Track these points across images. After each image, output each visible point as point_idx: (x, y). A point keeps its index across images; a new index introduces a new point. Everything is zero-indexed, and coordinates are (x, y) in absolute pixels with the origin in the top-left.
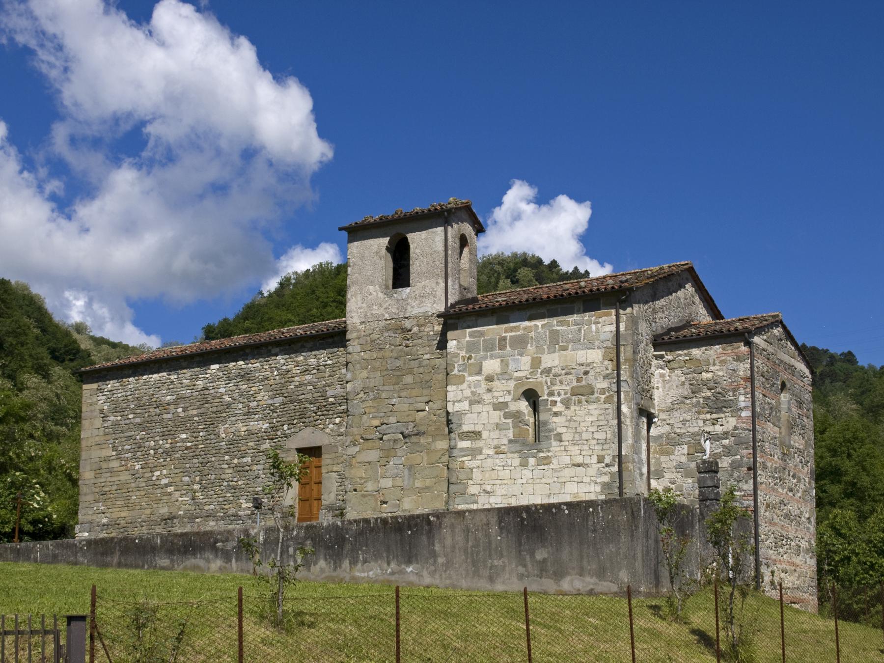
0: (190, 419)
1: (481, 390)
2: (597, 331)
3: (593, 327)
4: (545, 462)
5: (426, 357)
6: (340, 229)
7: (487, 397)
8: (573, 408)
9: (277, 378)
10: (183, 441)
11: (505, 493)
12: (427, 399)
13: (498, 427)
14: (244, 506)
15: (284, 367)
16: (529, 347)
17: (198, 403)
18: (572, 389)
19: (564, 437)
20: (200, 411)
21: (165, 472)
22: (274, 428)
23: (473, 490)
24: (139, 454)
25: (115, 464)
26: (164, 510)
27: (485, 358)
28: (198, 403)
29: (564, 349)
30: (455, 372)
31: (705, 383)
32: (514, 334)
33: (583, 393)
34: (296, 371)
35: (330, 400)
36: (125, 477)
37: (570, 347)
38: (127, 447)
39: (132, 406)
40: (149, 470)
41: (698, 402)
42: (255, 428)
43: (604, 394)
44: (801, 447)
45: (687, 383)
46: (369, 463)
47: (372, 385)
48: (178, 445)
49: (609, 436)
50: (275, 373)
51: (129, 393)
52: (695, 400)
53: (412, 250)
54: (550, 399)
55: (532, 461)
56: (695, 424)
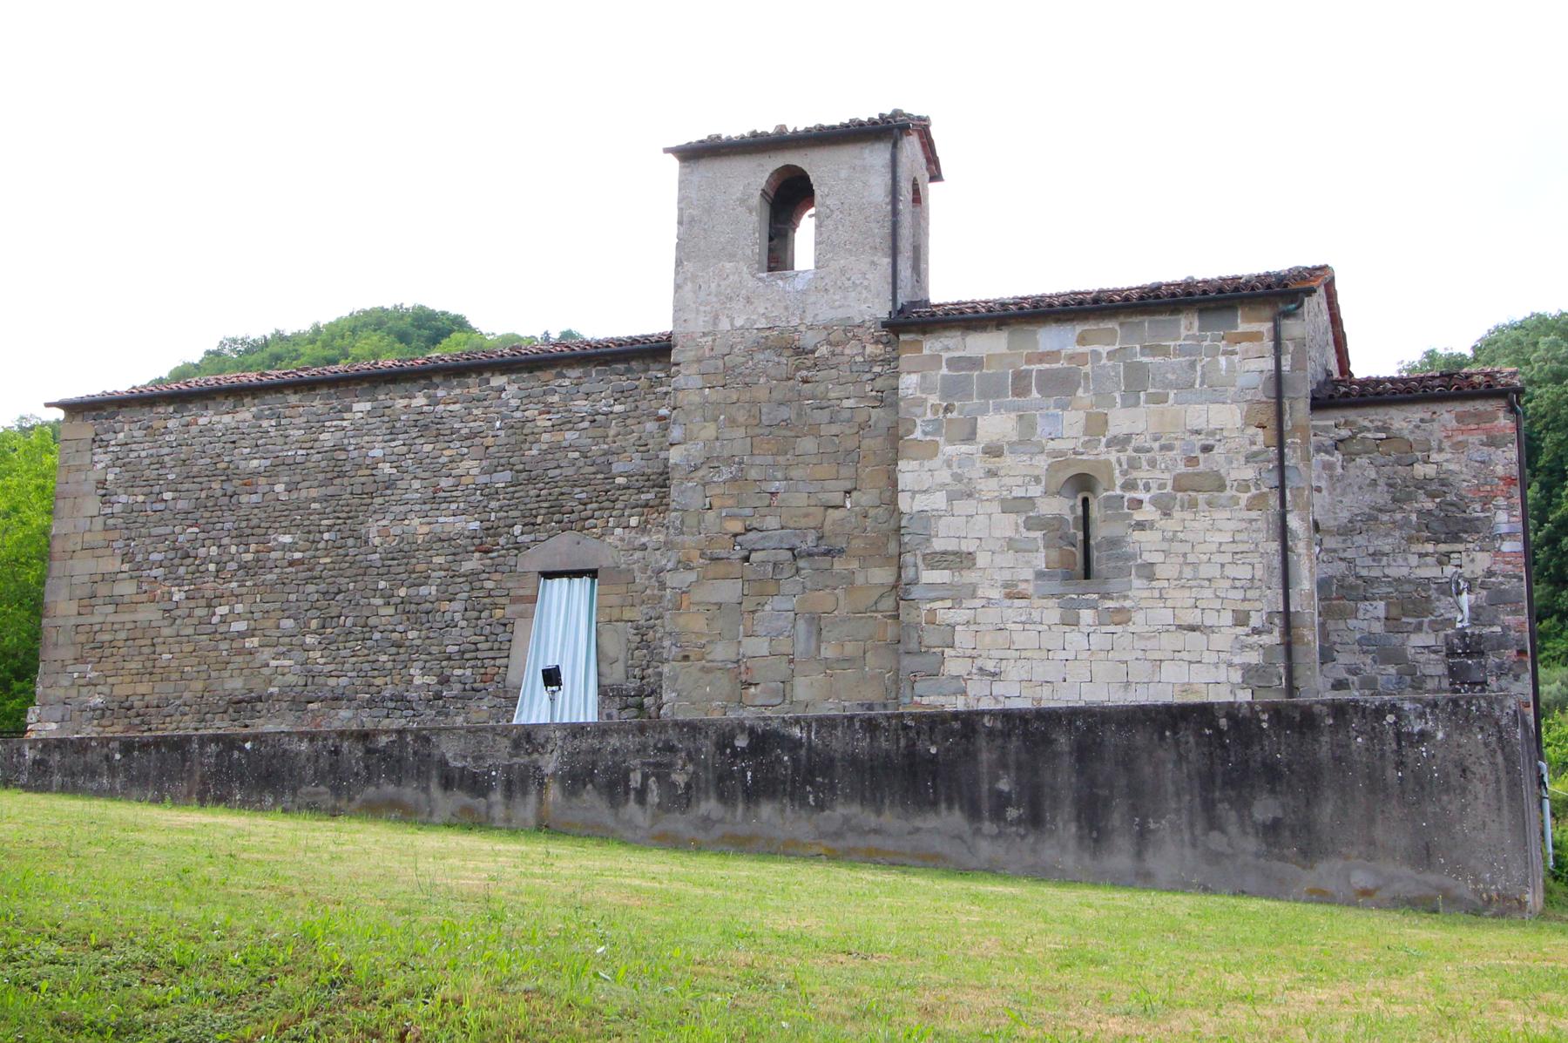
1: (976, 471)
2: (1231, 368)
3: (1222, 360)
4: (1117, 619)
6: (667, 151)
7: (989, 487)
9: (502, 433)
10: (284, 547)
11: (1025, 677)
12: (849, 485)
13: (1011, 544)
14: (417, 681)
15: (518, 414)
16: (1080, 392)
17: (321, 476)
18: (1177, 479)
19: (1160, 571)
20: (323, 491)
21: (239, 608)
23: (953, 667)
24: (182, 570)
25: (127, 588)
26: (235, 685)
27: (985, 411)
28: (321, 476)
29: (1160, 399)
30: (918, 434)
31: (1422, 484)
33: (1197, 485)
34: (543, 422)
35: (620, 480)
36: (148, 614)
37: (1172, 395)
38: (155, 557)
39: (170, 477)
40: (203, 602)
41: (1406, 520)
42: (447, 528)
43: (1248, 489)
45: (1382, 482)
46: (719, 605)
47: (726, 454)
48: (273, 555)
50: (498, 424)
51: (167, 450)
52: (1398, 516)
54: (1128, 495)
55: (1087, 616)
56: (1400, 561)
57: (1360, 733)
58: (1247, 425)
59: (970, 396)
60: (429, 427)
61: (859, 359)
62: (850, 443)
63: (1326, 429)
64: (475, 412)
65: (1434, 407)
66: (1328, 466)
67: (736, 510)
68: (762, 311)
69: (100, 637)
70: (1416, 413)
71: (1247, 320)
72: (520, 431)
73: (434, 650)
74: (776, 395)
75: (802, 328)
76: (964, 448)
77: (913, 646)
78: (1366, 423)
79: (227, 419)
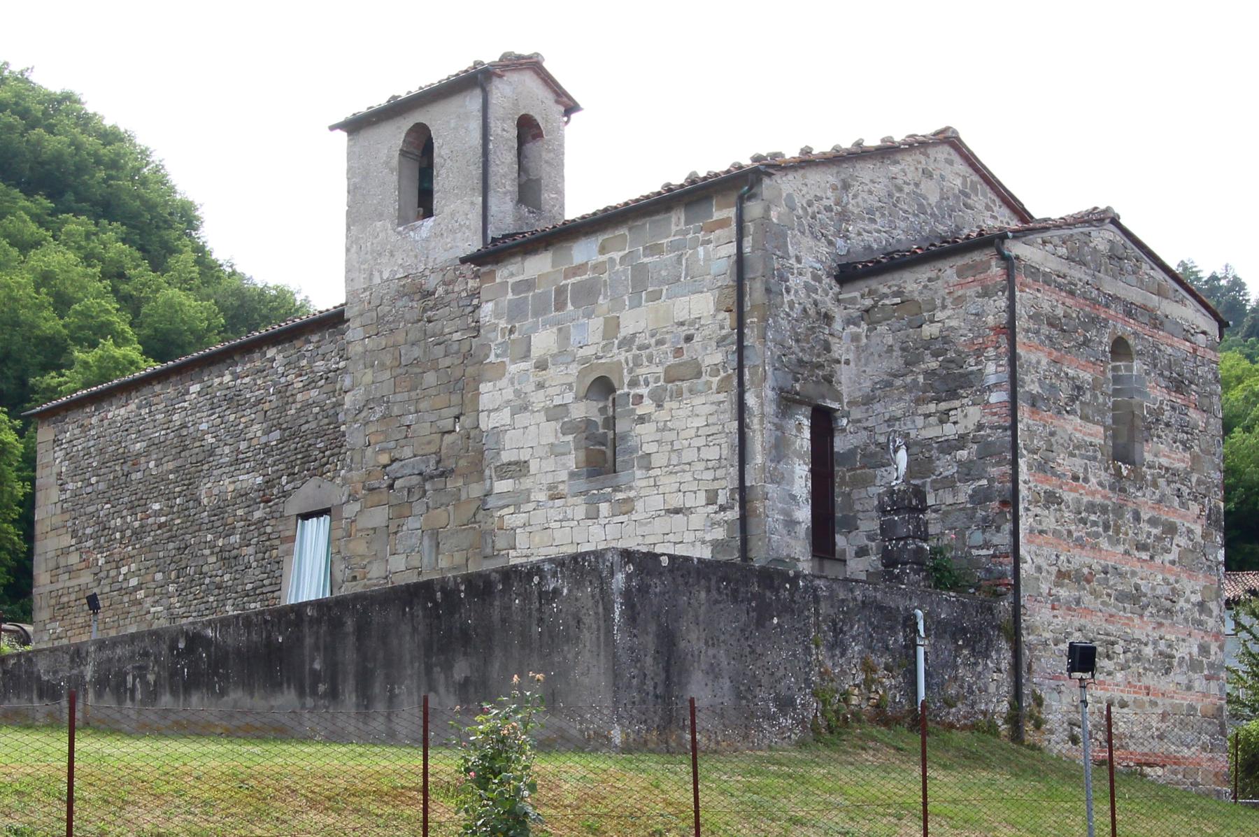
0: (163, 479)
2: (707, 259)
5: (456, 336)
6: (332, 128)
8: (667, 405)
9: (273, 398)
10: (157, 514)
12: (456, 411)
15: (283, 380)
16: (601, 300)
17: (174, 451)
18: (666, 372)
22: (269, 483)
27: (535, 328)
28: (174, 451)
29: (656, 296)
30: (492, 358)
31: (927, 344)
32: (578, 278)
33: (682, 375)
40: (114, 565)
44: (1181, 466)
45: (896, 348)
46: (374, 529)
47: (378, 395)
49: (725, 453)
52: (909, 379)
53: (436, 151)
57: (518, 595)
58: (718, 310)
59: (525, 317)
60: (234, 400)
61: (464, 294)
62: (458, 373)
63: (853, 301)
64: (259, 382)
65: (939, 265)
66: (855, 338)
67: (384, 445)
68: (400, 262)
69: (65, 599)
70: (924, 273)
71: (720, 208)
72: (284, 392)
73: (239, 588)
74: (411, 337)
75: (427, 272)
76: (523, 365)
77: (488, 551)
78: (886, 290)
79: (123, 411)
